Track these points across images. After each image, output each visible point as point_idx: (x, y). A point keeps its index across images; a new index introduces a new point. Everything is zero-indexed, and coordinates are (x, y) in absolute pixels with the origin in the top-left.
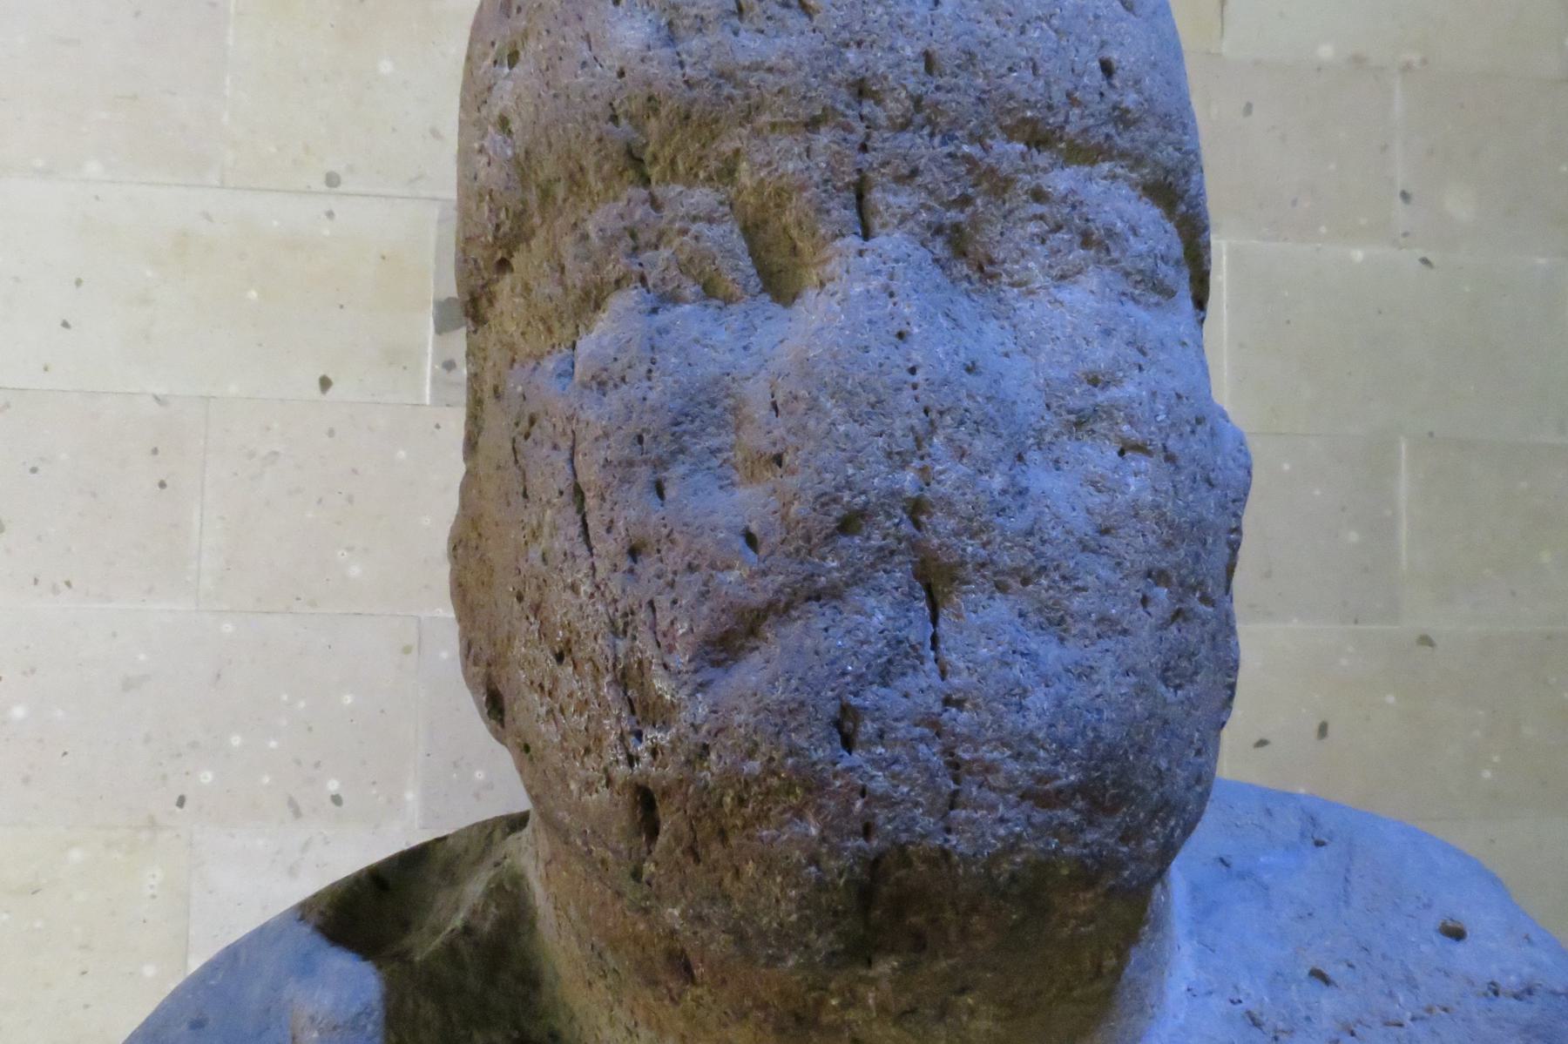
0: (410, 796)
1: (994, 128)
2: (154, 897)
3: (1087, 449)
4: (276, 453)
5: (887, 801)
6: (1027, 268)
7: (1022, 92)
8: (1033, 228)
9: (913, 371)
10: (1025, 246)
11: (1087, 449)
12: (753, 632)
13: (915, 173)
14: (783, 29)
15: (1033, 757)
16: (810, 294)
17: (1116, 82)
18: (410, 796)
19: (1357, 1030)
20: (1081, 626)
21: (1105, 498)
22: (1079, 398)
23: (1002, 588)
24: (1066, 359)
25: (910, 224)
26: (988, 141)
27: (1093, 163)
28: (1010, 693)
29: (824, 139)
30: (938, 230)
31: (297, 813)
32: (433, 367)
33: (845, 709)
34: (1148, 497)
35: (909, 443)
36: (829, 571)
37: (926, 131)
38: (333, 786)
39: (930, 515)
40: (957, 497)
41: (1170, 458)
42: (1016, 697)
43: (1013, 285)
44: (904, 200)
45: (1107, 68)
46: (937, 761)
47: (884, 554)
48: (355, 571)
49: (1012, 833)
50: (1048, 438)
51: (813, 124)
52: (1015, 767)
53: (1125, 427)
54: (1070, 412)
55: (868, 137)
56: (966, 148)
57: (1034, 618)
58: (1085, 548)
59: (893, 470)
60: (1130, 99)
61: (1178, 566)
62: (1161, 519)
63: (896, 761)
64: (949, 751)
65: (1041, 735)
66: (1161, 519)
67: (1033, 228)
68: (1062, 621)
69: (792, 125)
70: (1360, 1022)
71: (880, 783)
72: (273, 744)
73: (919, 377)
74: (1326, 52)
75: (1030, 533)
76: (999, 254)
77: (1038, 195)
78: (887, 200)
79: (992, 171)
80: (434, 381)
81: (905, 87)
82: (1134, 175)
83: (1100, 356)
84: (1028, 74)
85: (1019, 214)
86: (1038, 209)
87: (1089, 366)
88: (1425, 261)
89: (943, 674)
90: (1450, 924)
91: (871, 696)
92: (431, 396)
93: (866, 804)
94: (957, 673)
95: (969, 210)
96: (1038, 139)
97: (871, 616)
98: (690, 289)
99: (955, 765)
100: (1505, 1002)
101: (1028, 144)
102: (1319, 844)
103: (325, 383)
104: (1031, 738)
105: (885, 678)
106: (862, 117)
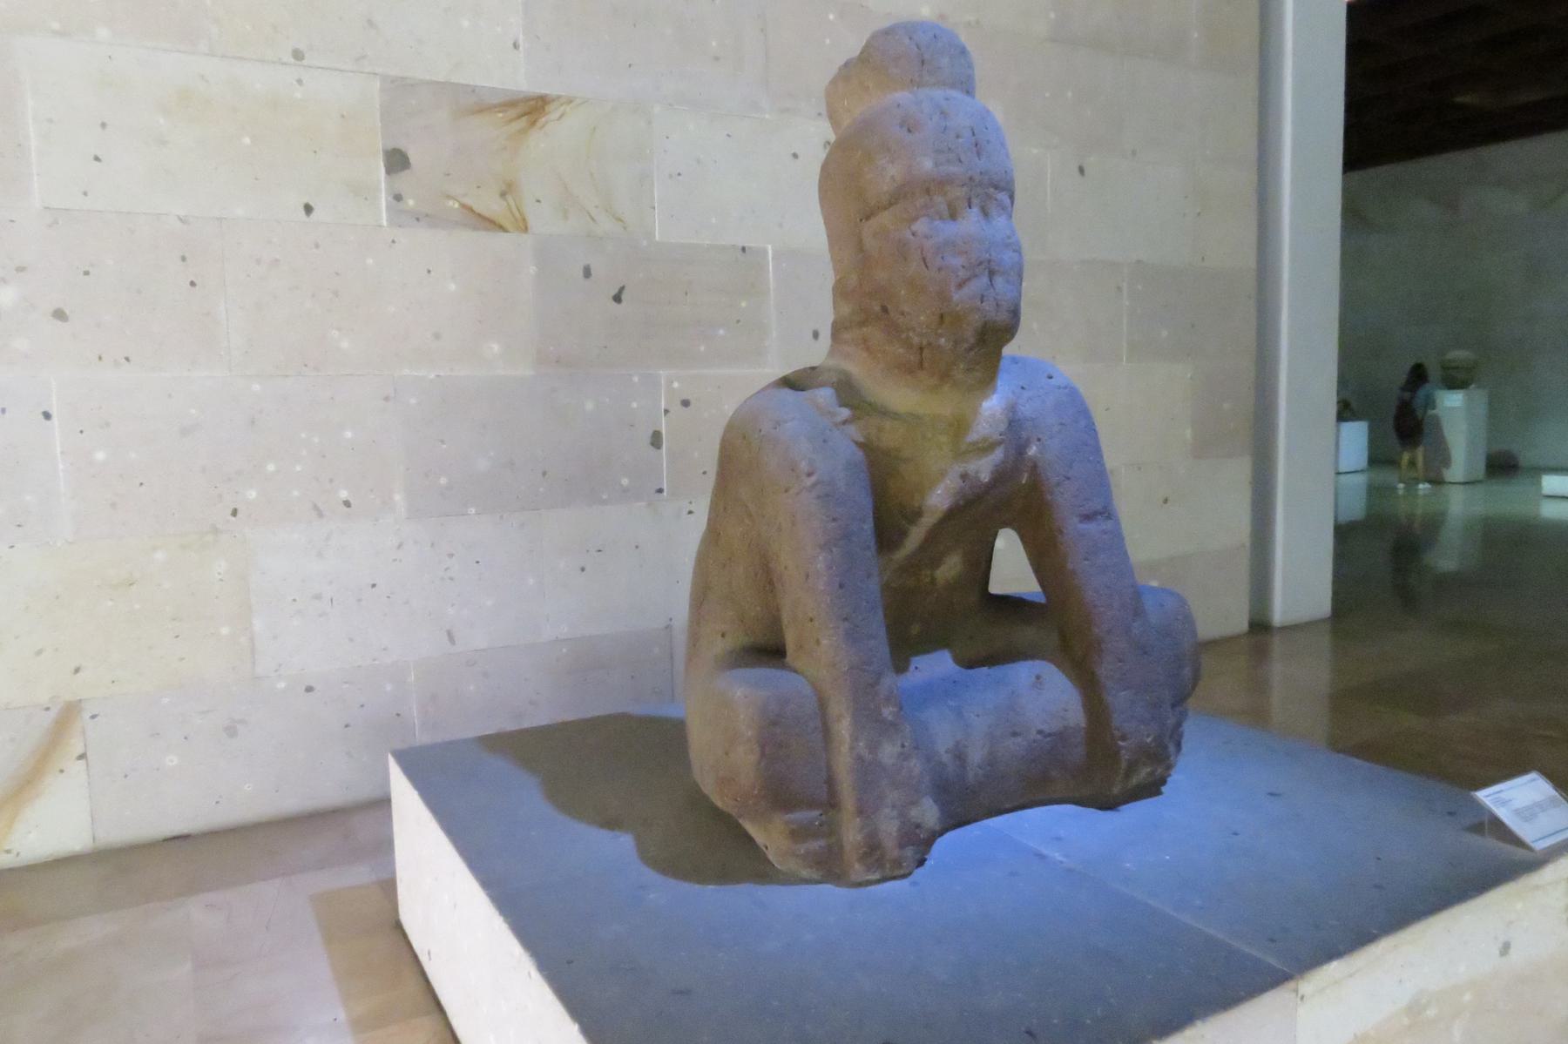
0: (397, 497)
2: (221, 580)
4: (277, 260)
12: (964, 283)
16: (960, 219)
18: (397, 497)
31: (321, 515)
32: (386, 200)
38: (344, 495)
48: (345, 344)
72: (298, 468)
77: (996, 200)
78: (975, 201)
80: (388, 208)
92: (387, 220)
96: (996, 187)
98: (937, 217)
103: (308, 209)
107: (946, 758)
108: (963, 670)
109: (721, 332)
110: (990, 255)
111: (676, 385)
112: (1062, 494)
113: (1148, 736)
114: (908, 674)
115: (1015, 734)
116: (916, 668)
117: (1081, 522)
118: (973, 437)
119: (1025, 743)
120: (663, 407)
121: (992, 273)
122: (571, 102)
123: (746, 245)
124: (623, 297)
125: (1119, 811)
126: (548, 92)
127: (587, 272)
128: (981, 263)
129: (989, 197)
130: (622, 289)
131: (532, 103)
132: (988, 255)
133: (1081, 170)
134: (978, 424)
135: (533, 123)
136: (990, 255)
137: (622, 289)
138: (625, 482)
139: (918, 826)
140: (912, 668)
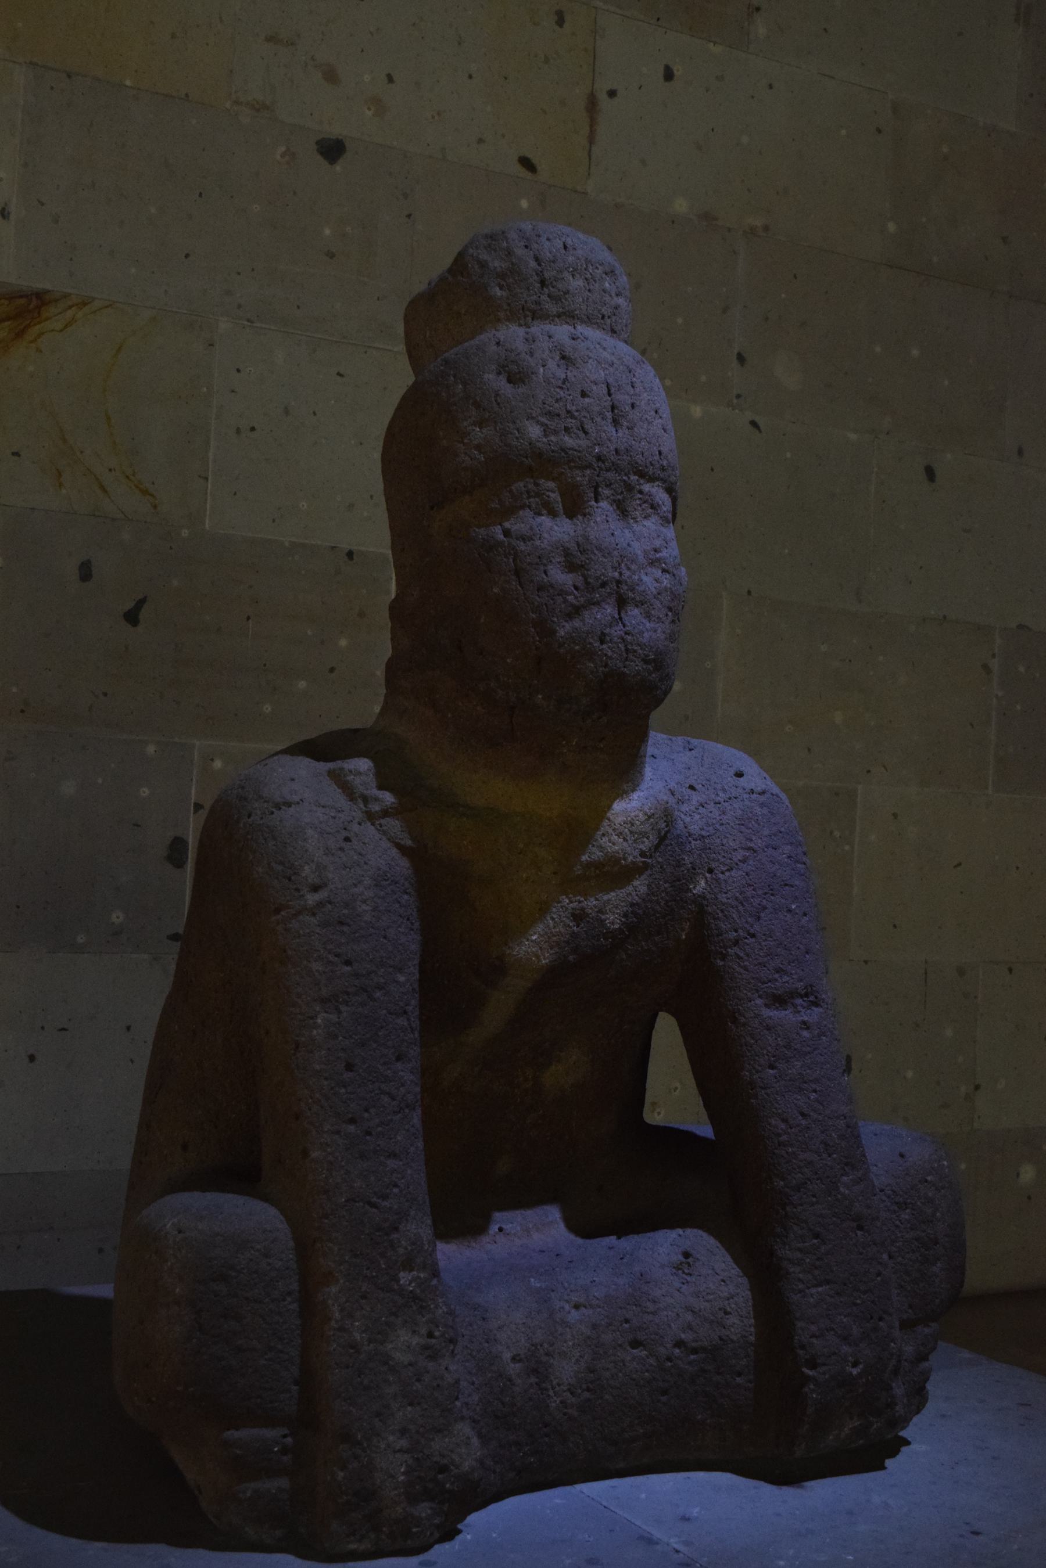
1: (631, 472)
3: (653, 570)
5: (611, 658)
6: (636, 514)
7: (639, 461)
8: (638, 502)
9: (617, 545)
10: (636, 507)
11: (653, 570)
13: (611, 484)
14: (578, 437)
15: (645, 650)
17: (662, 457)
19: (705, 805)
20: (654, 618)
21: (659, 585)
22: (652, 555)
23: (637, 606)
24: (648, 544)
25: (609, 500)
26: (629, 476)
27: (654, 482)
28: (640, 632)
29: (588, 472)
30: (614, 501)
33: (602, 633)
34: (669, 586)
35: (617, 565)
36: (597, 597)
37: (614, 472)
39: (621, 584)
40: (628, 580)
41: (674, 575)
42: (641, 633)
43: (632, 519)
44: (607, 492)
45: (660, 453)
46: (623, 649)
47: (610, 594)
49: (639, 669)
50: (644, 566)
51: (586, 467)
52: (640, 651)
53: (663, 565)
54: (650, 559)
55: (600, 472)
56: (624, 478)
57: (644, 615)
58: (655, 598)
59: (613, 571)
60: (665, 463)
61: (674, 607)
62: (672, 592)
63: (614, 647)
64: (626, 646)
65: (647, 644)
66: (672, 592)
67: (638, 502)
68: (650, 616)
69: (580, 467)
70: (706, 803)
71: (610, 653)
73: (618, 547)
74: (681, 206)
75: (644, 591)
76: (629, 509)
77: (641, 492)
79: (630, 485)
81: (610, 459)
82: (664, 485)
83: (658, 543)
84: (641, 456)
85: (636, 497)
86: (640, 496)
87: (654, 546)
88: (754, 424)
89: (624, 626)
90: (739, 772)
91: (607, 631)
93: (606, 659)
94: (628, 626)
95: (622, 495)
96: (642, 475)
97: (607, 610)
99: (627, 650)
100: (754, 796)
101: (639, 477)
102: (691, 750)
104: (645, 644)
105: (611, 627)
106: (598, 467)
107: (514, 1369)
108: (580, 1241)
109: (302, 684)
110: (621, 574)
111: (218, 764)
112: (740, 958)
113: (855, 1365)
114: (485, 1239)
115: (636, 1344)
116: (501, 1229)
117: (766, 1005)
118: (593, 854)
119: (652, 1361)
120: (193, 801)
121: (622, 603)
122: (85, 304)
123: (354, 548)
124: (144, 614)
125: (802, 1487)
126: (48, 286)
127: (86, 572)
128: (604, 585)
129: (629, 488)
130: (141, 603)
131: (23, 301)
132: (616, 574)
133: (930, 473)
134: (347, 763)
135: (20, 334)
136: (621, 574)
137: (141, 603)
138: (117, 917)
139: (443, 1469)
140: (494, 1228)
